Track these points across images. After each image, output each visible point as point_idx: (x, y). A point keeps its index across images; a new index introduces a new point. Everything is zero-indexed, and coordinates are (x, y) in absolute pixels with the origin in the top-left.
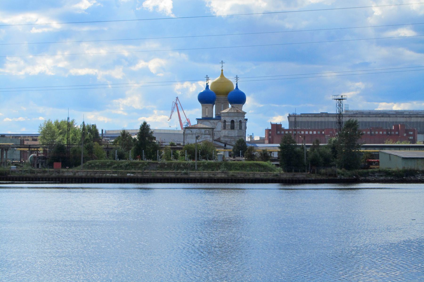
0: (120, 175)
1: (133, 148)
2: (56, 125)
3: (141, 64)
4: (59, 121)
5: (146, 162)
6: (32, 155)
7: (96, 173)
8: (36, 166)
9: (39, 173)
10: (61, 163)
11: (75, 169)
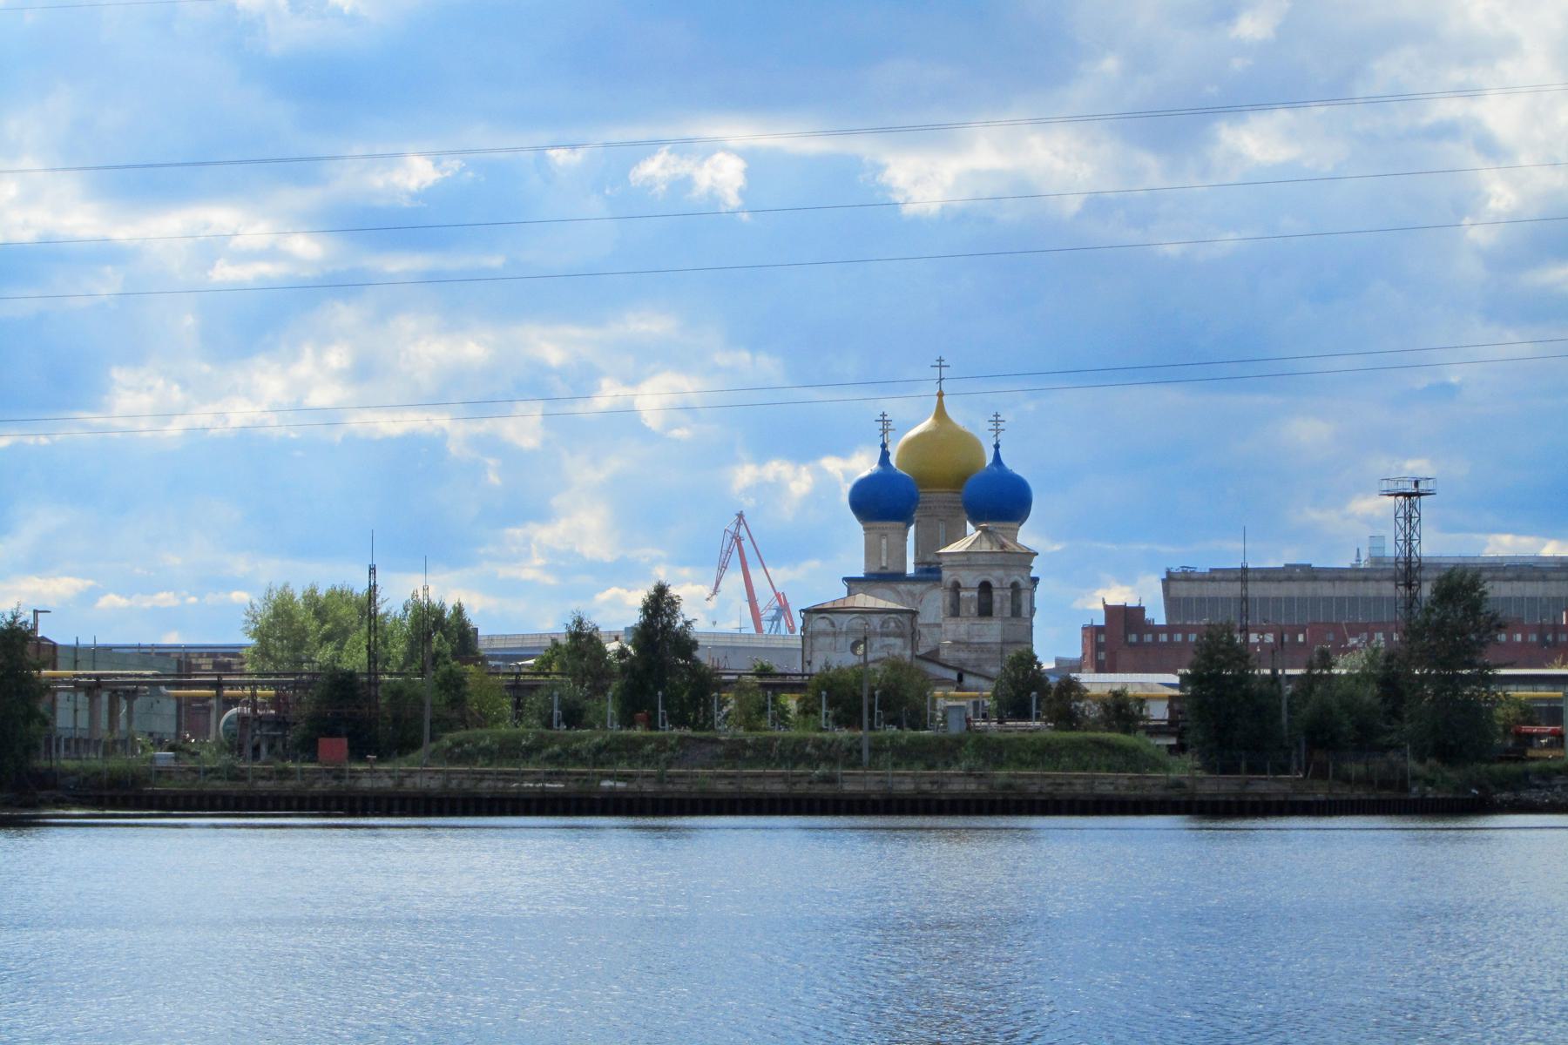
0: (573, 786)
1: (616, 684)
2: (308, 605)
3: (609, 394)
4: (322, 592)
5: (672, 737)
6: (234, 710)
7: (481, 780)
8: (248, 751)
9: (263, 778)
10: (345, 741)
11: (401, 765)
